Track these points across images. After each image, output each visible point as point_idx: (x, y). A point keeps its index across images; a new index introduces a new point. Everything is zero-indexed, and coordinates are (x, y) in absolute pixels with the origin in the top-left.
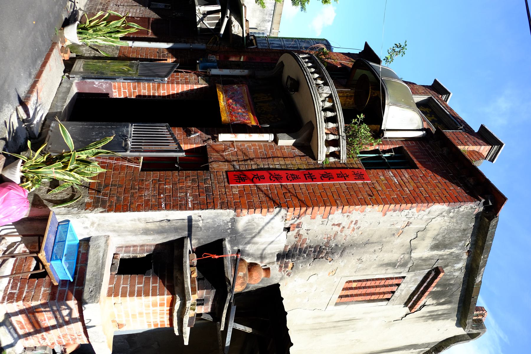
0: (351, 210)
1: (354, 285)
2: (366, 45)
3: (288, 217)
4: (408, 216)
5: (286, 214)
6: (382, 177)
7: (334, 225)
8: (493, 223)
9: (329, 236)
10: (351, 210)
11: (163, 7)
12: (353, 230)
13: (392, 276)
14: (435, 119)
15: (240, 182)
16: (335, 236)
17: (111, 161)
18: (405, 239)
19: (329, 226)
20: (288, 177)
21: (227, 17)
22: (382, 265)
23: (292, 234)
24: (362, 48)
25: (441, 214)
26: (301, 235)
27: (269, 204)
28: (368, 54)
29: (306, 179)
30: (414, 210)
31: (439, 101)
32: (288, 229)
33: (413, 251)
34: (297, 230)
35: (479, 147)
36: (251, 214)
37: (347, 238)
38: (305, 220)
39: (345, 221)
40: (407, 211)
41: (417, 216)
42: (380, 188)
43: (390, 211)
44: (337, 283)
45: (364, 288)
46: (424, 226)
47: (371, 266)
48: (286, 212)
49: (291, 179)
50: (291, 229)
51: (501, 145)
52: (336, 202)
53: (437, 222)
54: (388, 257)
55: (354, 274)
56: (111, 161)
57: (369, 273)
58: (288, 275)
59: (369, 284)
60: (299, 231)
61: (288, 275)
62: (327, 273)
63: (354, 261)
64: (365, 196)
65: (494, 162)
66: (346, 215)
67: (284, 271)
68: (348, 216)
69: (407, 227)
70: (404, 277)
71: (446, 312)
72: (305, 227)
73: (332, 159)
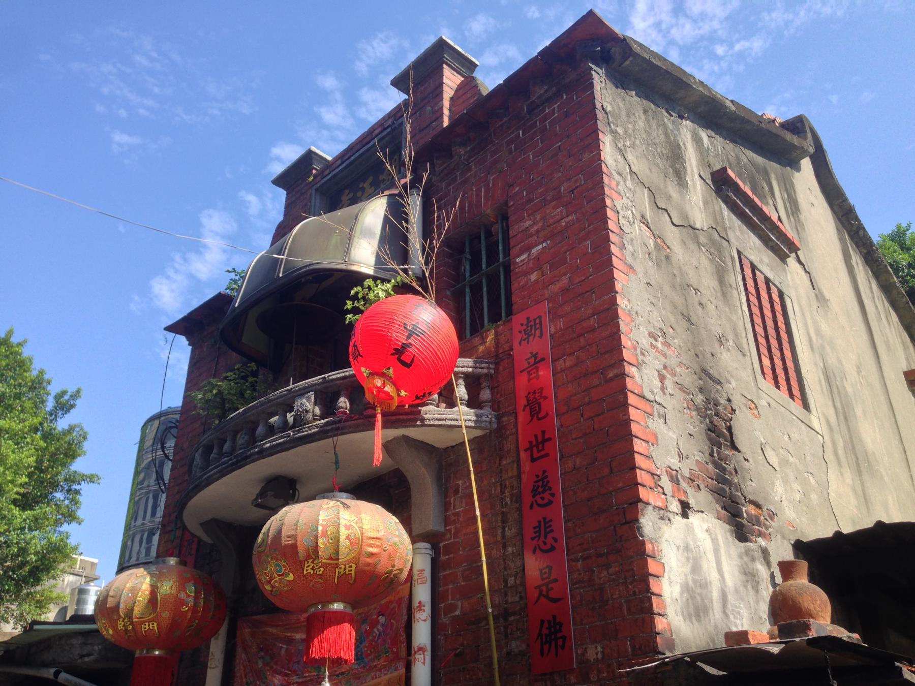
1: (766, 362)
2: (173, 328)
3: (660, 504)
4: (631, 220)
6: (534, 277)
7: (663, 389)
8: (635, 47)
13: (740, 277)
14: (370, 179)
15: (564, 638)
18: (673, 236)
20: (540, 502)
21: (57, 674)
22: (724, 295)
23: (694, 497)
24: (182, 340)
25: (620, 150)
29: (547, 455)
30: (619, 204)
31: (327, 172)
32: (685, 509)
33: (692, 223)
35: (445, 88)
36: (665, 607)
37: (685, 362)
39: (653, 363)
40: (622, 221)
41: (629, 201)
42: (565, 280)
43: (623, 255)
44: (769, 400)
45: (767, 338)
46: (646, 191)
47: (730, 320)
48: (650, 508)
49: (547, 495)
50: (683, 498)
51: (441, 45)
52: (612, 379)
53: (635, 162)
54: (707, 282)
55: (748, 358)
57: (741, 325)
58: (772, 515)
59: (760, 330)
60: (683, 477)
61: (772, 515)
62: (755, 420)
63: (724, 354)
64: (590, 311)
65: (477, 63)
66: (640, 358)
67: (767, 528)
68: (643, 354)
69: (650, 225)
70: (739, 253)
71: (782, 184)
72: (674, 462)
73: (486, 394)
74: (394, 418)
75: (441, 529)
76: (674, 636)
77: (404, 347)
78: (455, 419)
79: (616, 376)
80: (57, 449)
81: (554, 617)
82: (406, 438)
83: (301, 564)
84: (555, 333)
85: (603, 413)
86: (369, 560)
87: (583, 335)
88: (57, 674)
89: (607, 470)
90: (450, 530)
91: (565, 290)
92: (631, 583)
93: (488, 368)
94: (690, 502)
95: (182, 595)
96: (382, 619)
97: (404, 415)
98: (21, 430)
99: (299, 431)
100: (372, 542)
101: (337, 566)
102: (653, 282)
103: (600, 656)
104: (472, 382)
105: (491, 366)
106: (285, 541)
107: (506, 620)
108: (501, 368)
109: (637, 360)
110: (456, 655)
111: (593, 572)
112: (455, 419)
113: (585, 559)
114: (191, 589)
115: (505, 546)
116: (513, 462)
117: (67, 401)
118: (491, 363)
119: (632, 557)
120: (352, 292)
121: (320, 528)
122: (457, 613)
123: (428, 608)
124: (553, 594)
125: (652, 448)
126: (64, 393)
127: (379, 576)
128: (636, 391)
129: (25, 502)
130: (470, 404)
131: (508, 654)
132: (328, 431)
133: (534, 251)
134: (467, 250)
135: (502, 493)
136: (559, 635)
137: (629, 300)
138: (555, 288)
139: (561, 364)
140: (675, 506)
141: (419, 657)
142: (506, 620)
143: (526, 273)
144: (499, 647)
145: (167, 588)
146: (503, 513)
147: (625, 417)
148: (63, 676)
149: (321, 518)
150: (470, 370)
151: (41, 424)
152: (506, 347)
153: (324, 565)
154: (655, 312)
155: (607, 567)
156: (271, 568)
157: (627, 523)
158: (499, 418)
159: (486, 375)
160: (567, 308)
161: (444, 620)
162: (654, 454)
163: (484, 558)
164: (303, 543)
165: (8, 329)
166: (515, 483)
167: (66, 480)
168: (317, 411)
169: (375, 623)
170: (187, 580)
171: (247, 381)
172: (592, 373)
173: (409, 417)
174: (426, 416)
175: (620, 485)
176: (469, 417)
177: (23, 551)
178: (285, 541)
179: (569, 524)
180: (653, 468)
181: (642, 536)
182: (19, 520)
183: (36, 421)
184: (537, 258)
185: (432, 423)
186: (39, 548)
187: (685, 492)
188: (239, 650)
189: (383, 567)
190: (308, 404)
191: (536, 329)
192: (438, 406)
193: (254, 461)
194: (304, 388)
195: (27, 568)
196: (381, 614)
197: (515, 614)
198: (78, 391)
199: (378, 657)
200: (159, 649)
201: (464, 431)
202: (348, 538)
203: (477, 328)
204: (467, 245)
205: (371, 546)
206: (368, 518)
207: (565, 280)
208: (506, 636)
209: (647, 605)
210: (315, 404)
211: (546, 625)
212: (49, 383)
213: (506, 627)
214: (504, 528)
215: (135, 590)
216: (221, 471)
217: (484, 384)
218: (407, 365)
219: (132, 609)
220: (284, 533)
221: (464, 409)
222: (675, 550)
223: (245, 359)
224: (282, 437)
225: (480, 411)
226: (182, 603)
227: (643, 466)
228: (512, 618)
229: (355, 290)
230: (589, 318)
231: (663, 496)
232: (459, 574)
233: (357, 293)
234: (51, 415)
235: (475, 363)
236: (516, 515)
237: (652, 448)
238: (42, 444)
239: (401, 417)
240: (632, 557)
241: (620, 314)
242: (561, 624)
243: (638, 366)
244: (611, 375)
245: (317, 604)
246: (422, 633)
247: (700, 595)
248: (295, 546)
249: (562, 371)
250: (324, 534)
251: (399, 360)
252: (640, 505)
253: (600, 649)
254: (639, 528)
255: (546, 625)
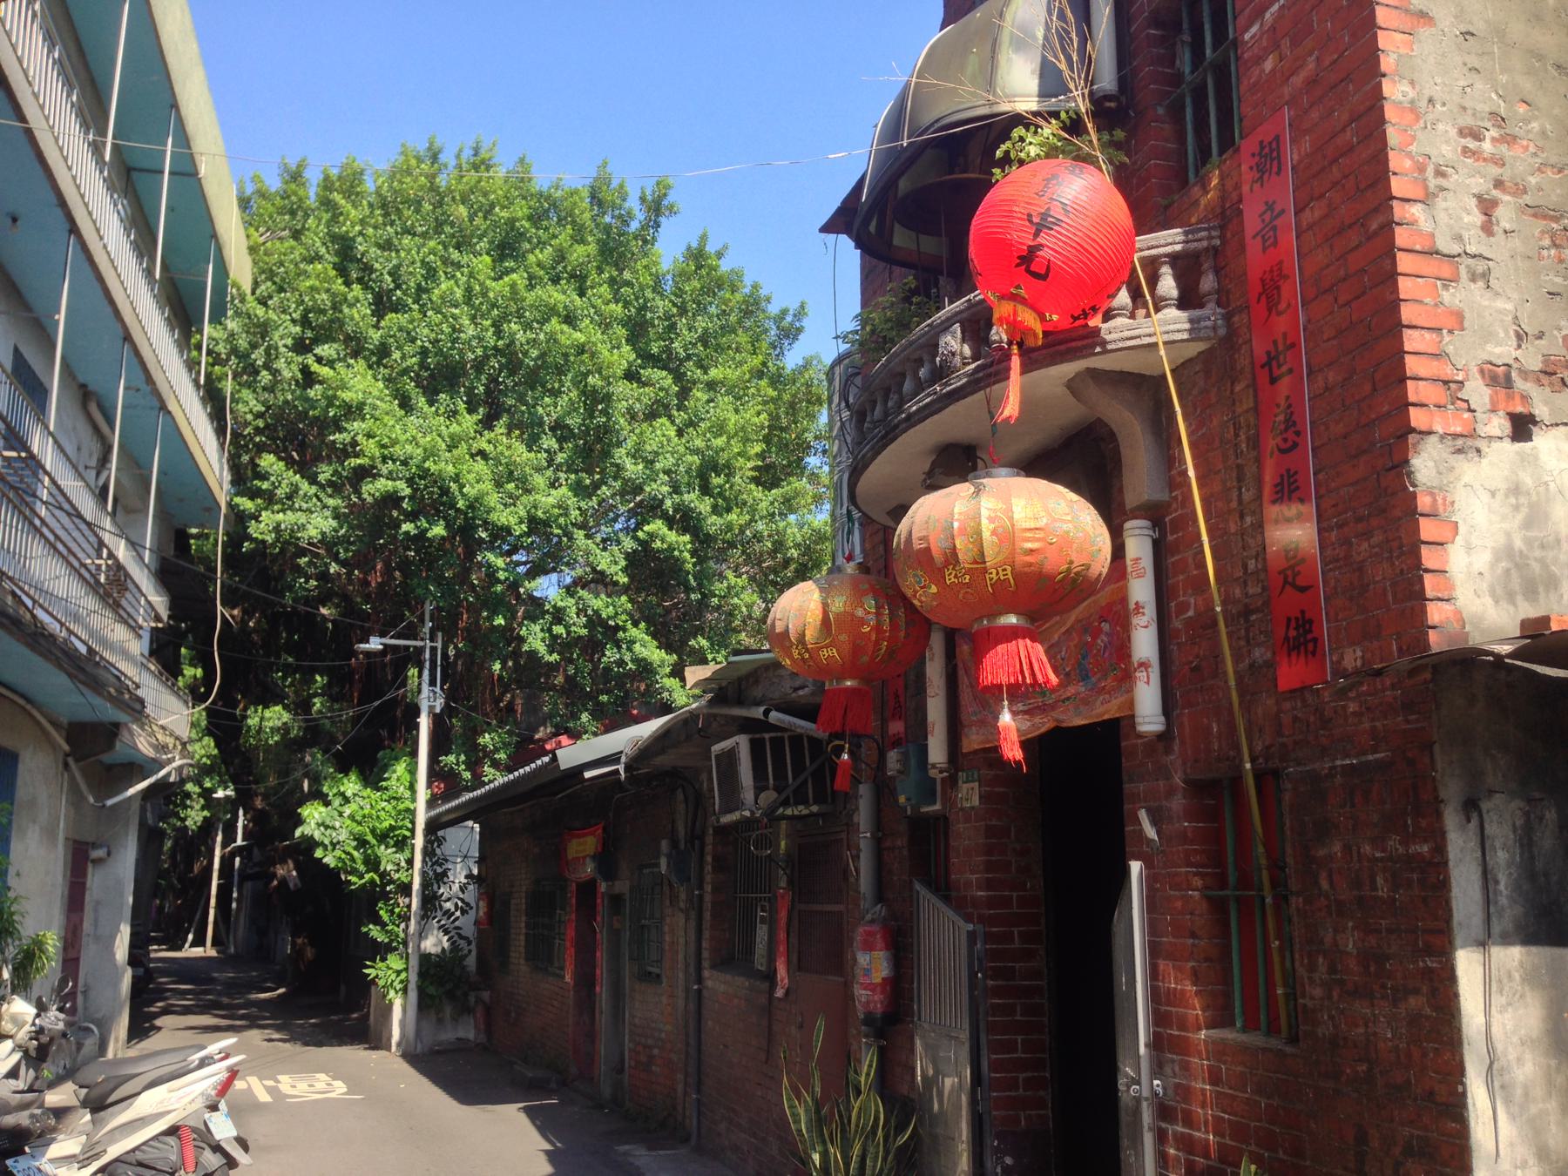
0: (1408, 163)
2: (827, 228)
5: (1442, 437)
6: (1268, 65)
7: (1488, 229)
9: (1547, 242)
10: (1408, 163)
11: (765, 928)
12: (1509, 139)
15: (1315, 640)
16: (1545, 217)
17: (707, 904)
19: (1498, 248)
21: (766, 713)
23: (1546, 403)
26: (1546, 362)
27: (1397, 512)
28: (844, 220)
34: (1520, 384)
36: (1452, 587)
37: (1553, 160)
38: (1467, 354)
39: (1472, 181)
42: (1311, 64)
48: (1433, 439)
49: (1290, 435)
52: (1376, 233)
56: (707, 904)
60: (1525, 374)
64: (1345, 117)
66: (1433, 182)
68: (1440, 173)
72: (1503, 350)
73: (1208, 283)
74: (1063, 347)
75: (1164, 496)
76: (1467, 629)
77: (1033, 250)
78: (1151, 330)
79: (1382, 227)
80: (794, 396)
81: (1303, 612)
82: (1093, 373)
83: (941, 571)
84: (1300, 162)
85: (1364, 293)
86: (1029, 559)
87: (1335, 160)
88: (766, 713)
89: (1368, 387)
90: (1175, 498)
91: (1311, 82)
92: (1398, 557)
93: (1210, 238)
94: (1536, 412)
95: (860, 613)
96: (1106, 627)
97: (1071, 340)
98: (740, 378)
99: (946, 384)
100: (1029, 535)
101: (985, 571)
102: (1479, 26)
103: (1359, 663)
104: (1185, 266)
105: (1214, 233)
106: (917, 545)
107: (1247, 621)
108: (1229, 235)
109: (1426, 188)
110: (1192, 670)
111: (1351, 544)
112: (1151, 330)
113: (1340, 526)
114: (870, 603)
115: (1242, 517)
116: (1248, 386)
117: (791, 324)
118: (1213, 228)
119: (1400, 518)
120: (999, 154)
121: (956, 525)
122: (1191, 613)
123: (1150, 612)
124: (1300, 582)
125: (1447, 339)
126: (784, 312)
127: (1051, 577)
128: (1418, 247)
129: (767, 477)
130: (1183, 303)
131: (1252, 666)
132: (978, 381)
133: (1267, 15)
134: (1185, 26)
135: (1237, 435)
136: (1309, 637)
137: (1412, 83)
138: (1298, 80)
139: (1307, 216)
140: (1498, 425)
141: (1141, 675)
142: (1247, 621)
143: (1259, 60)
144: (1237, 659)
145: (838, 604)
146: (1239, 466)
147: (1393, 297)
148: (775, 716)
149: (956, 510)
150: (1178, 247)
151: (764, 364)
152: (1234, 196)
153: (969, 571)
154: (1479, 86)
155: (1366, 535)
156: (911, 580)
157: (1393, 468)
158: (1228, 318)
159: (1207, 249)
160: (1315, 115)
161: (1177, 624)
162: (1450, 349)
163: (1205, 538)
164: (938, 546)
165: (700, 233)
166: (1252, 421)
167: (816, 438)
168: (967, 351)
169: (1096, 633)
170: (864, 593)
171: (911, 303)
172: (1350, 227)
173: (1085, 342)
174: (1108, 338)
175: (1386, 409)
176: (1178, 326)
177: (779, 545)
178: (917, 545)
179: (1321, 476)
180: (1448, 372)
181: (1414, 486)
182: (764, 505)
183: (756, 361)
184: (1273, 29)
185: (1121, 345)
186: (799, 539)
187: (1525, 398)
188: (961, 672)
189: (1054, 563)
190: (953, 342)
191: (1272, 160)
192: (1132, 316)
193: (905, 431)
194: (948, 319)
195: (793, 567)
196: (1102, 619)
197: (1257, 610)
198: (802, 307)
199: (1105, 676)
200: (851, 677)
201: (1162, 352)
202: (994, 533)
203: (1180, 178)
204: (1184, 15)
205: (1028, 540)
206: (1022, 502)
207: (1311, 64)
208: (1248, 642)
209: (1417, 588)
210: (963, 340)
211: (1293, 624)
212: (768, 300)
213: (1247, 630)
214: (1240, 489)
215: (801, 611)
216: (872, 448)
217: (1206, 266)
218: (1044, 277)
219: (804, 635)
220: (914, 536)
221: (1172, 313)
222: (1485, 497)
223: (89, 668)
224: (929, 395)
225: (1198, 313)
226: (862, 622)
227: (1422, 373)
228: (1254, 617)
229: (1003, 147)
230: (1343, 130)
231: (1466, 415)
232: (1190, 560)
233: (1007, 153)
234: (775, 348)
235: (1186, 233)
236: (1254, 469)
237: (1447, 339)
238: (772, 393)
239: (1074, 344)
240: (1400, 518)
241: (1390, 113)
242: (1311, 622)
243: (1427, 199)
244: (1374, 226)
245: (981, 618)
246: (1144, 643)
247: (1542, 561)
248: (928, 550)
249: (1310, 227)
250: (962, 531)
251: (1028, 271)
252: (1412, 438)
253: (1359, 653)
254: (1410, 474)
255: (1293, 624)
